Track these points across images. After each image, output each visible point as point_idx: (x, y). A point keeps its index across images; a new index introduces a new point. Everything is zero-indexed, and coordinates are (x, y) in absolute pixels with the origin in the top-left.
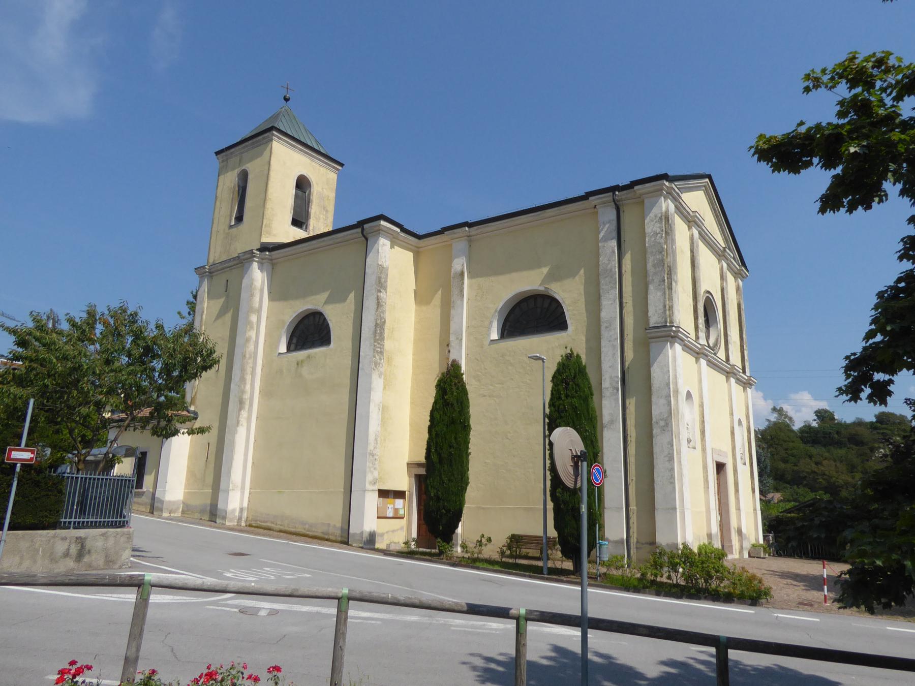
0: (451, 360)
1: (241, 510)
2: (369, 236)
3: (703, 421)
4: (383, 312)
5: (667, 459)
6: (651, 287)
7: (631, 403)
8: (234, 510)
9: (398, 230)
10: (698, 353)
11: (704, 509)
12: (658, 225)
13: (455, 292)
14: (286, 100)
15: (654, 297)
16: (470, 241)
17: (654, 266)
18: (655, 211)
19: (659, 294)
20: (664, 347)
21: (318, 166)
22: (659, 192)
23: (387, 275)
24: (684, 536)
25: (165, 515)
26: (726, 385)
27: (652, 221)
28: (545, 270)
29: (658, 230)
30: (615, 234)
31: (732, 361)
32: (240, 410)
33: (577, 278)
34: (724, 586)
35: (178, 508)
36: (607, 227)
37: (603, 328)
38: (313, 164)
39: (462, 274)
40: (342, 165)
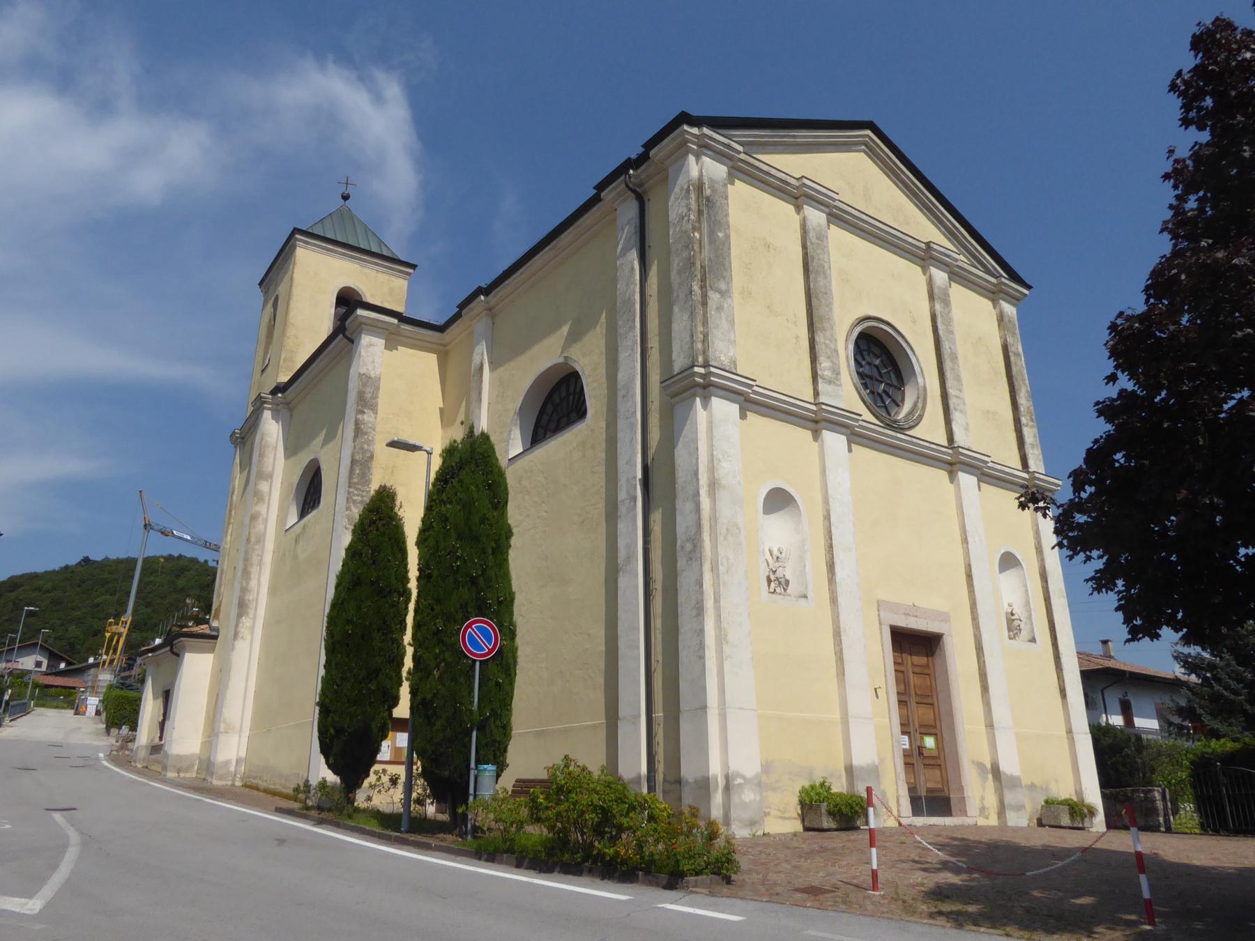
0: (374, 487)
1: (238, 761)
2: (353, 337)
3: (831, 546)
4: (369, 442)
5: (694, 613)
6: (676, 309)
7: (657, 517)
8: (227, 763)
9: (395, 321)
10: (816, 422)
11: (837, 716)
12: (684, 202)
13: (474, 396)
14: (346, 197)
15: (680, 323)
16: (493, 317)
17: (679, 273)
18: (682, 181)
19: (686, 317)
20: (691, 406)
21: (373, 273)
22: (682, 150)
23: (378, 388)
24: (725, 763)
25: (171, 775)
26: (951, 487)
27: (677, 199)
28: (565, 329)
29: (685, 210)
30: (635, 240)
31: (1032, 468)
32: (240, 616)
33: (598, 329)
34: (625, 847)
35: (192, 766)
36: (626, 232)
37: (620, 398)
38: (367, 271)
39: (481, 368)
40: (414, 266)
